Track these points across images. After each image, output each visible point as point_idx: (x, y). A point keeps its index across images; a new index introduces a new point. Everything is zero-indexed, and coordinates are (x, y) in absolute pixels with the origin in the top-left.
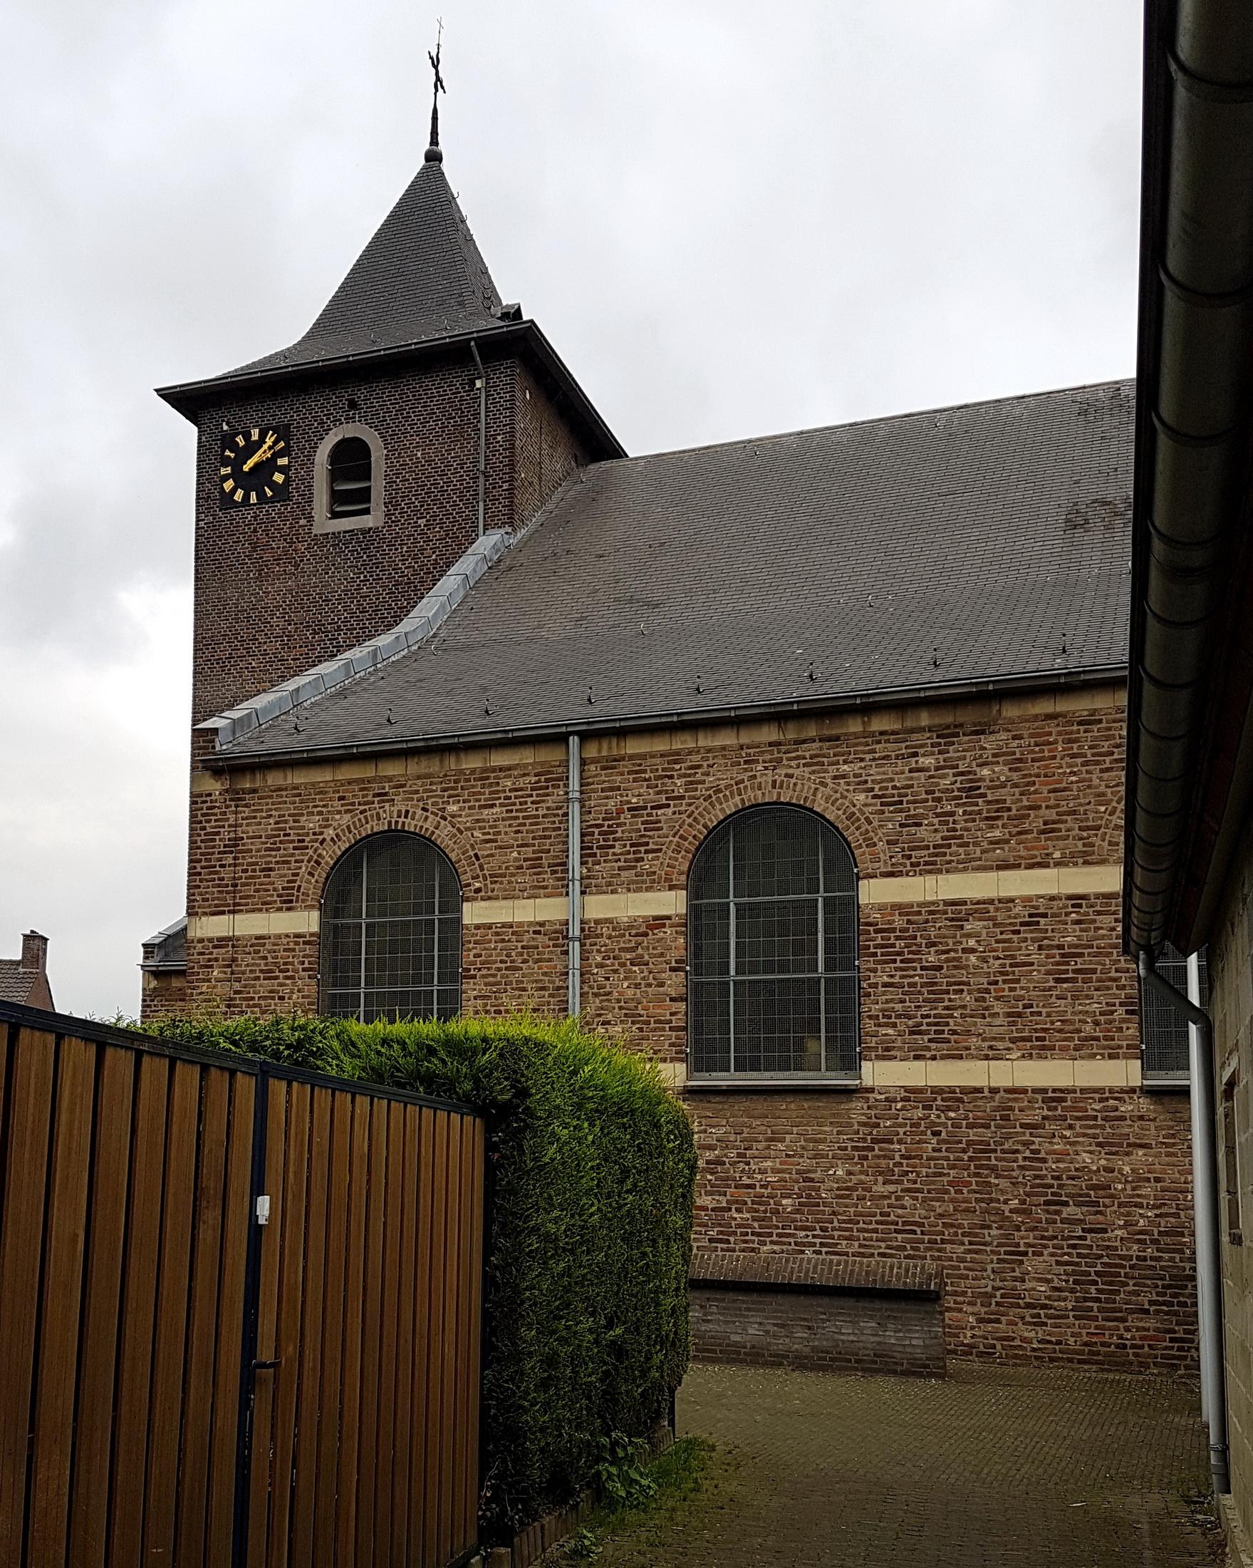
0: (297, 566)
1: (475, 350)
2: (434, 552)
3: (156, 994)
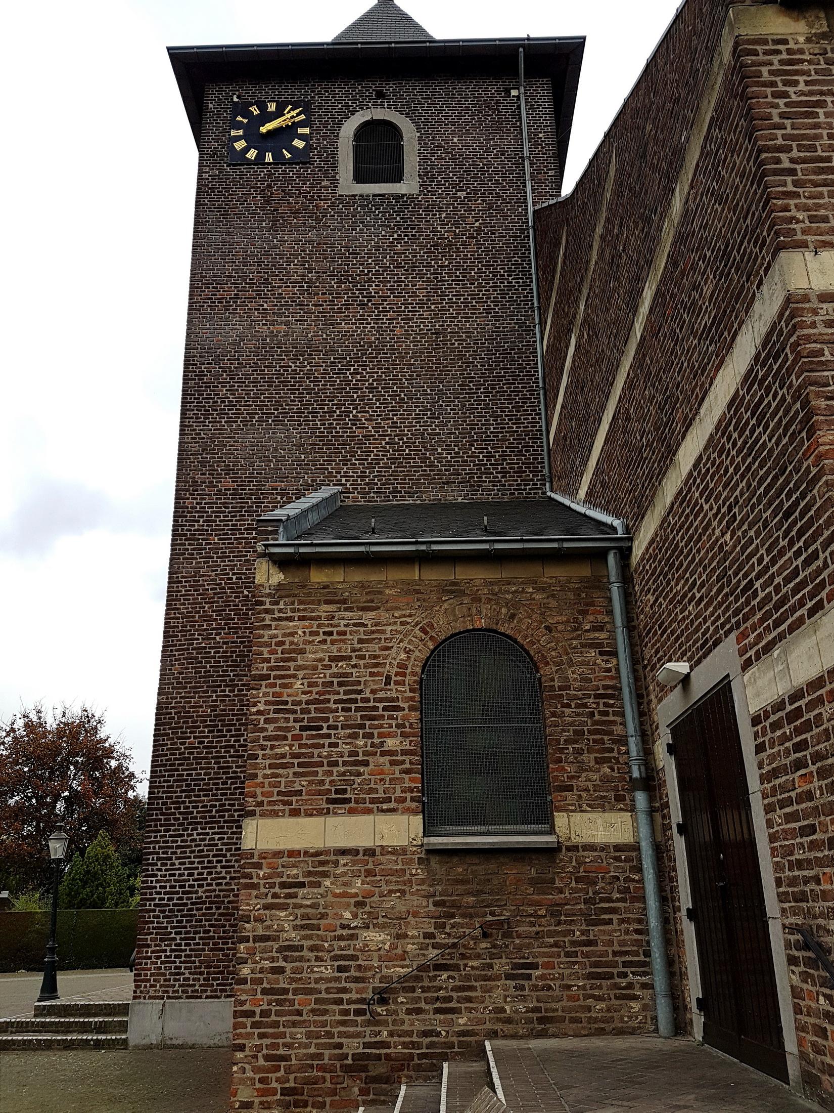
0: (318, 220)
1: (522, 55)
2: (476, 221)
3: (283, 593)
